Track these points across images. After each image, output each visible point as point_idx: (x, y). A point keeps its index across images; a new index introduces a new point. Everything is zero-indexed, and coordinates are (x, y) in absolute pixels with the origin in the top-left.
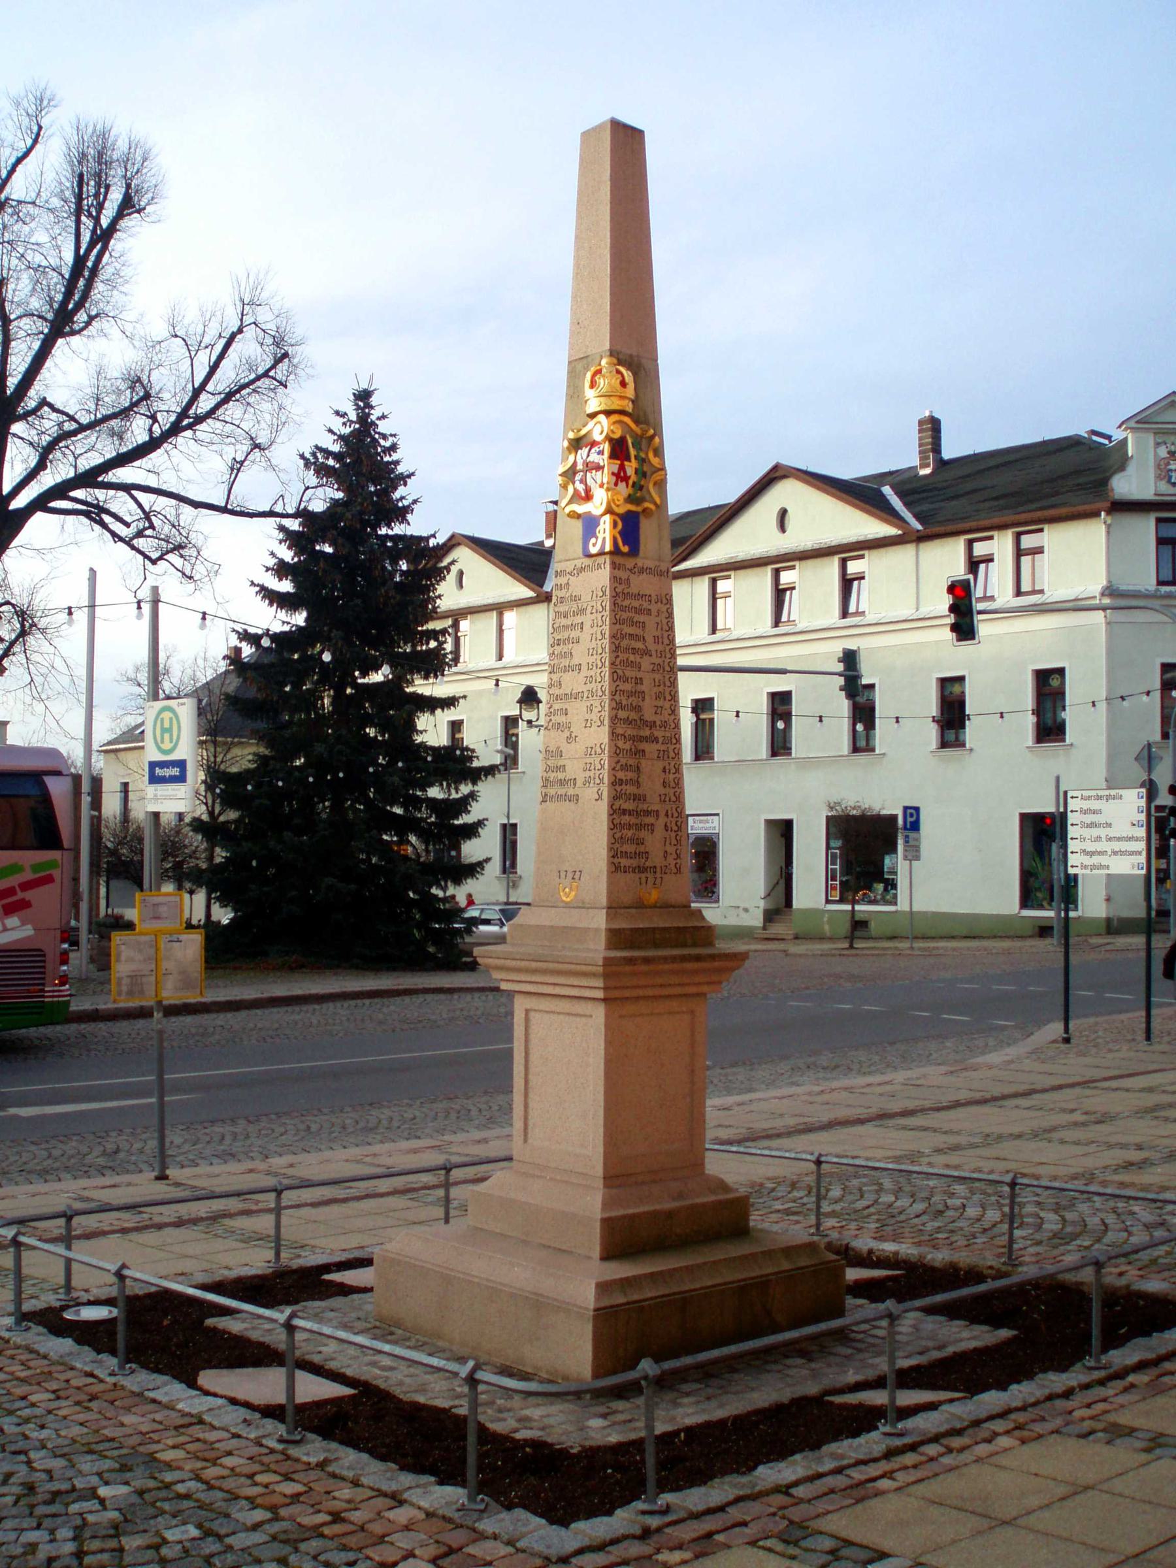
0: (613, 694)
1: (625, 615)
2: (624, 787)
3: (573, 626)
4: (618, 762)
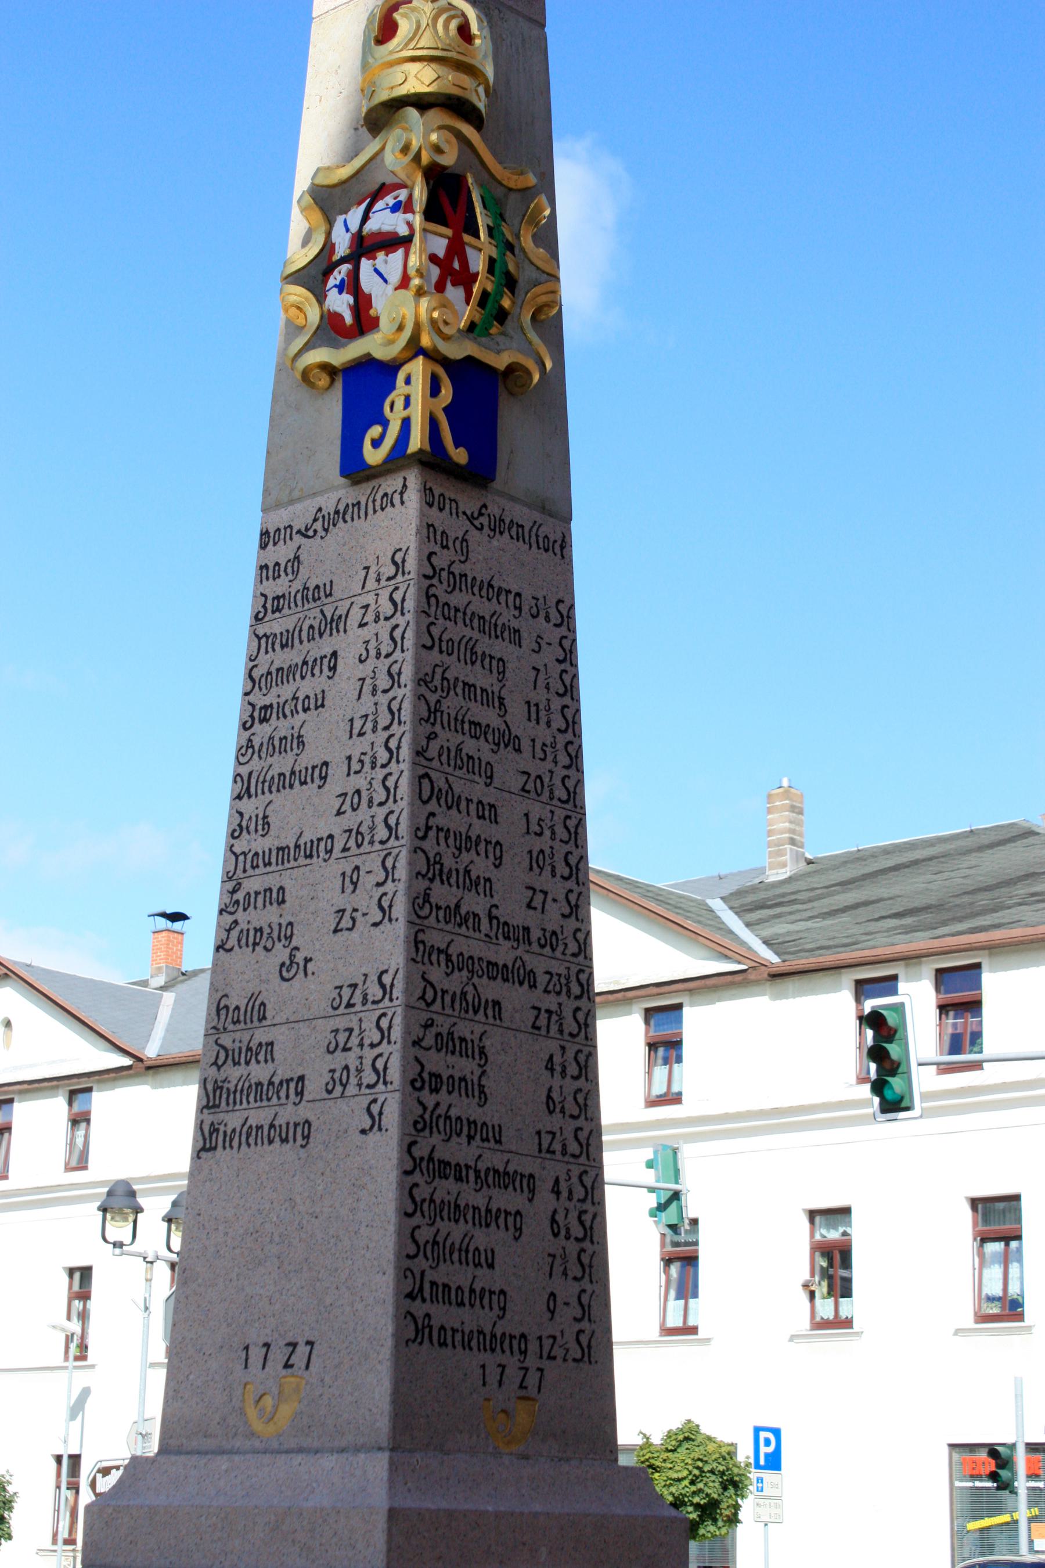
0: (421, 833)
1: (456, 631)
2: (443, 1096)
3: (306, 667)
4: (428, 1025)
